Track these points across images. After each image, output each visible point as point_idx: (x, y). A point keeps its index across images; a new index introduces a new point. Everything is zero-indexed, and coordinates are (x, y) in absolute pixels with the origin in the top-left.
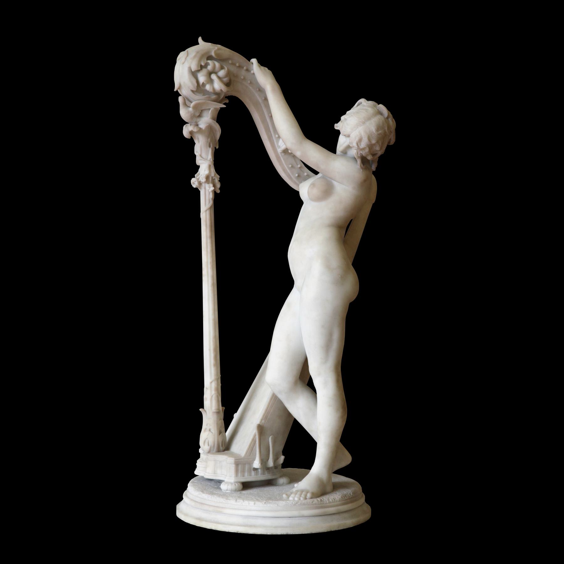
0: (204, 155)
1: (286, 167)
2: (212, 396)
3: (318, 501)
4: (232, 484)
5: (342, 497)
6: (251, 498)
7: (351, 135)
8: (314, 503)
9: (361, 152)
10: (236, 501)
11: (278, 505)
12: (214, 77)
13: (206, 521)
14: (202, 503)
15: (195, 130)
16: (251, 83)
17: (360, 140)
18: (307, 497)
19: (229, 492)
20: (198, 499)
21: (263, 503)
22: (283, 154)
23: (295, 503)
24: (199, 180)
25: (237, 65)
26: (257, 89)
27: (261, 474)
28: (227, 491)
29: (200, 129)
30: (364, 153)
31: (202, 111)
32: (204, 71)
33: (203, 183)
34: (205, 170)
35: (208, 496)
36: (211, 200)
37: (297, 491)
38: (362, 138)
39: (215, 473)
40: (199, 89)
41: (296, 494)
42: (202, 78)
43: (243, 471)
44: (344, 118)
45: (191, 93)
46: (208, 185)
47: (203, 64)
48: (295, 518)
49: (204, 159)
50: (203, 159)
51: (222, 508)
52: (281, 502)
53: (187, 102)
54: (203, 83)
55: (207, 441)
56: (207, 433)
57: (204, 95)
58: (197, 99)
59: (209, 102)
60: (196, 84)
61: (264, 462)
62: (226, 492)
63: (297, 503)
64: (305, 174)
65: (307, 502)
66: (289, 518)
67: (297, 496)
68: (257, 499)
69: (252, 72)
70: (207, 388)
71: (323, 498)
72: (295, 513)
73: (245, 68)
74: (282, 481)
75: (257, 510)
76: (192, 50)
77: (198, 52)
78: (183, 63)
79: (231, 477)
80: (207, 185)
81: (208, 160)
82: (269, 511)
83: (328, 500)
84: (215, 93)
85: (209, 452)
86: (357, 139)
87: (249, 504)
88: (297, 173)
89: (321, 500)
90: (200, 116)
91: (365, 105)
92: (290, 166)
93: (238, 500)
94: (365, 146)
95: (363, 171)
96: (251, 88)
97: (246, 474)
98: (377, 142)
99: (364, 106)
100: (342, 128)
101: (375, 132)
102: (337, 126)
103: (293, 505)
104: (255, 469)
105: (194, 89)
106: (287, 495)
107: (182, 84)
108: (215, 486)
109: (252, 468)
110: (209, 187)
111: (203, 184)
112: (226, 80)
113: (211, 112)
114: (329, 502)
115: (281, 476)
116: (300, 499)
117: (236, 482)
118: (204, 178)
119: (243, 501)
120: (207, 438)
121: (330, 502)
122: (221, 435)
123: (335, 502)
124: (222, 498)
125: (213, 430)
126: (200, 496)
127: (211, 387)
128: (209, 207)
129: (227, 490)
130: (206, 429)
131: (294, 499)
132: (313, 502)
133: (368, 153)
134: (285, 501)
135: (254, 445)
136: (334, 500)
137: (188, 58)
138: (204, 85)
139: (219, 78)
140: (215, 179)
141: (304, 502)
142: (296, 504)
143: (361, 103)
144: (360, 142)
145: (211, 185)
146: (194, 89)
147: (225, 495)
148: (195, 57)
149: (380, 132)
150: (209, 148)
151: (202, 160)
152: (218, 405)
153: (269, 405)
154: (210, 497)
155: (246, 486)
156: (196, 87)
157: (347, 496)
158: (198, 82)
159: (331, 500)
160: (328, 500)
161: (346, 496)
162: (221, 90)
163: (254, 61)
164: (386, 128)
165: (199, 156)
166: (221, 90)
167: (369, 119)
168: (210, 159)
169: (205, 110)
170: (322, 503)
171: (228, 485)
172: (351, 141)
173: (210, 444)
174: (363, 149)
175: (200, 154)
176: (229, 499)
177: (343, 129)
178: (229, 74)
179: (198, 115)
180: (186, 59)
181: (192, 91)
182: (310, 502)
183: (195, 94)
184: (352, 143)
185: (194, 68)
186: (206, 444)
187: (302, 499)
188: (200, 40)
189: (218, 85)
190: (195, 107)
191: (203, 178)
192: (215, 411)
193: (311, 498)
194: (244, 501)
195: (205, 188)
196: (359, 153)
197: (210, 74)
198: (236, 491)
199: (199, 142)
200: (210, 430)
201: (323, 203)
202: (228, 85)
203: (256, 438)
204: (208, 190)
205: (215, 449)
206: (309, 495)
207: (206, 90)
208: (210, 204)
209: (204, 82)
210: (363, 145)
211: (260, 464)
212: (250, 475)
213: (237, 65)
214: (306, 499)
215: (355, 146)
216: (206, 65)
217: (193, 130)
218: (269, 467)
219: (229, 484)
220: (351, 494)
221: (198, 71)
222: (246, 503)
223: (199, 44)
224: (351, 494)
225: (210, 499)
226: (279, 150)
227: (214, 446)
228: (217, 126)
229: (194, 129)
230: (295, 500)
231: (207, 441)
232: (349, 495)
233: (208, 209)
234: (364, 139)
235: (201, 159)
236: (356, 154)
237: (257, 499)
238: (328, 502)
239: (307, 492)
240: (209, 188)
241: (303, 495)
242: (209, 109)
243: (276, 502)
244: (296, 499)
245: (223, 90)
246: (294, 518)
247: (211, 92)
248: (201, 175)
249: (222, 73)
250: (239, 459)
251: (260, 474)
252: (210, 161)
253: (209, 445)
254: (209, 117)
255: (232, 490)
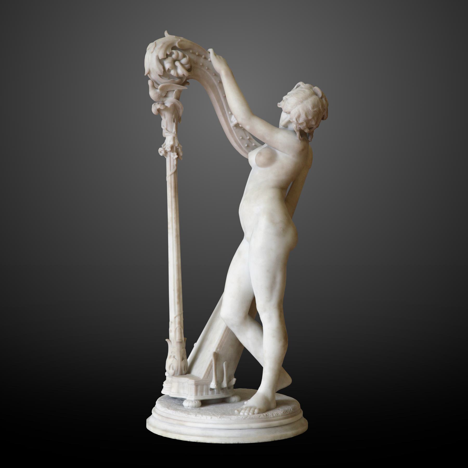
0: (169, 129)
1: (237, 138)
2: (176, 329)
3: (264, 415)
4: (192, 402)
5: (284, 412)
6: (209, 413)
7: (291, 112)
8: (260, 417)
9: (300, 126)
10: (196, 416)
11: (230, 419)
12: (177, 63)
13: (171, 432)
14: (167, 418)
15: (162, 108)
16: (208, 69)
17: (299, 116)
18: (255, 413)
19: (190, 408)
20: (164, 414)
21: (219, 417)
22: (235, 128)
23: (245, 417)
24: (165, 150)
25: (197, 54)
26: (214, 74)
27: (217, 393)
28: (188, 408)
29: (166, 107)
30: (302, 127)
31: (168, 92)
32: (170, 59)
33: (168, 152)
34: (170, 141)
35: (173, 411)
36: (175, 166)
37: (247, 407)
38: (300, 114)
39: (178, 392)
40: (165, 73)
41: (246, 410)
42: (167, 65)
43: (202, 391)
44: (286, 98)
45: (159, 77)
46: (173, 153)
47: (168, 53)
48: (245, 430)
49: (169, 132)
50: (168, 132)
51: (185, 421)
52: (233, 416)
53: (155, 85)
54: (169, 69)
55: (171, 366)
56: (172, 359)
57: (169, 79)
58: (163, 82)
59: (174, 84)
60: (163, 70)
61: (219, 383)
62: (187, 409)
63: (246, 418)
64: (253, 144)
65: (255, 417)
66: (240, 430)
67: (247, 411)
68: (213, 414)
69: (209, 60)
70: (172, 322)
71: (268, 414)
72: (245, 426)
73: (203, 56)
74: (234, 399)
75: (213, 424)
76: (160, 42)
77: (164, 43)
78: (152, 53)
79: (192, 396)
80: (172, 154)
81: (173, 133)
82: (223, 424)
83: (272, 415)
84: (179, 77)
85: (174, 375)
86: (296, 116)
87: (207, 418)
88: (246, 144)
89: (266, 415)
90: (166, 96)
91: (303, 87)
92: (241, 138)
93: (197, 415)
94: (303, 121)
95: (301, 141)
96: (208, 73)
97: (204, 393)
98: (313, 118)
99: (302, 88)
100: (284, 106)
101: (311, 110)
102: (280, 105)
103: (243, 419)
104: (212, 390)
105: (161, 74)
106: (238, 410)
107: (151, 70)
108: (179, 404)
109: (209, 389)
110: (173, 155)
111: (169, 153)
112: (187, 66)
113: (175, 93)
114: (273, 417)
115: (233, 395)
116: (249, 414)
117: (196, 400)
118: (170, 148)
119: (202, 416)
120: (172, 364)
121: (273, 417)
122: (183, 361)
123: (278, 417)
124: (185, 413)
125: (176, 357)
126: (166, 411)
127: (175, 321)
128: (174, 172)
129: (188, 407)
130: (171, 356)
131: (244, 414)
132: (259, 417)
133: (305, 127)
134: (237, 416)
135: (211, 369)
136: (277, 415)
137: (156, 48)
138: (169, 70)
139: (182, 65)
140: (178, 149)
141: (252, 417)
142: (246, 418)
143: (300, 86)
144: (299, 118)
145: (175, 154)
146: (161, 74)
147: (186, 411)
148: (162, 47)
149: (315, 109)
150: (173, 123)
151: (167, 133)
152: (181, 336)
153: (223, 336)
154: (174, 412)
155: (204, 403)
156: (163, 72)
157: (288, 412)
158: (164, 68)
159: (274, 415)
160: (272, 415)
161: (287, 412)
162: (184, 75)
163: (211, 50)
164: (320, 107)
165: (165, 129)
166: (184, 75)
167: (306, 99)
168: (175, 132)
169: (170, 91)
170: (267, 417)
171: (189, 403)
172: (291, 117)
173: (174, 369)
174: (301, 124)
175: (166, 128)
176: (190, 414)
177: (285, 107)
178: (190, 61)
179: (164, 95)
180: (154, 49)
181: (160, 76)
182: (257, 416)
183: (162, 78)
184: (292, 119)
185: (161, 56)
186: (171, 369)
187: (250, 414)
188: (166, 33)
189: (181, 71)
190: (162, 89)
191: (168, 148)
192: (178, 341)
193: (258, 413)
194: (203, 415)
195: (170, 156)
196: (298, 127)
197: (174, 61)
198: (196, 407)
199: (165, 118)
200: (174, 357)
201: (268, 169)
202: (189, 70)
203: (212, 363)
204: (173, 158)
205: (179, 373)
206: (256, 411)
207: (171, 75)
208: (174, 169)
209: (170, 68)
210: (301, 120)
211: (215, 385)
212: (208, 394)
213: (197, 54)
214: (254, 414)
215: (295, 121)
216: (171, 54)
217: (160, 108)
218: (224, 387)
219: (190, 402)
220: (292, 410)
221: (165, 59)
222: (204, 417)
223: (165, 37)
224: (292, 410)
225: (174, 414)
226: (232, 125)
227: (178, 370)
228: (180, 104)
229: (161, 107)
230: (245, 415)
231: (171, 366)
232: (290, 411)
233: (173, 173)
234: (302, 115)
235: (167, 132)
236: (296, 127)
237: (213, 414)
238: (272, 417)
239: (255, 409)
240: (173, 156)
241: (251, 411)
242: (174, 91)
243: (229, 416)
244: (246, 414)
245: (185, 75)
246: (244, 430)
247: (175, 77)
248: (167, 145)
249: (184, 61)
250: (198, 381)
251: (215, 394)
252: (174, 133)
253: (173, 369)
254: (174, 97)
255: (192, 407)
